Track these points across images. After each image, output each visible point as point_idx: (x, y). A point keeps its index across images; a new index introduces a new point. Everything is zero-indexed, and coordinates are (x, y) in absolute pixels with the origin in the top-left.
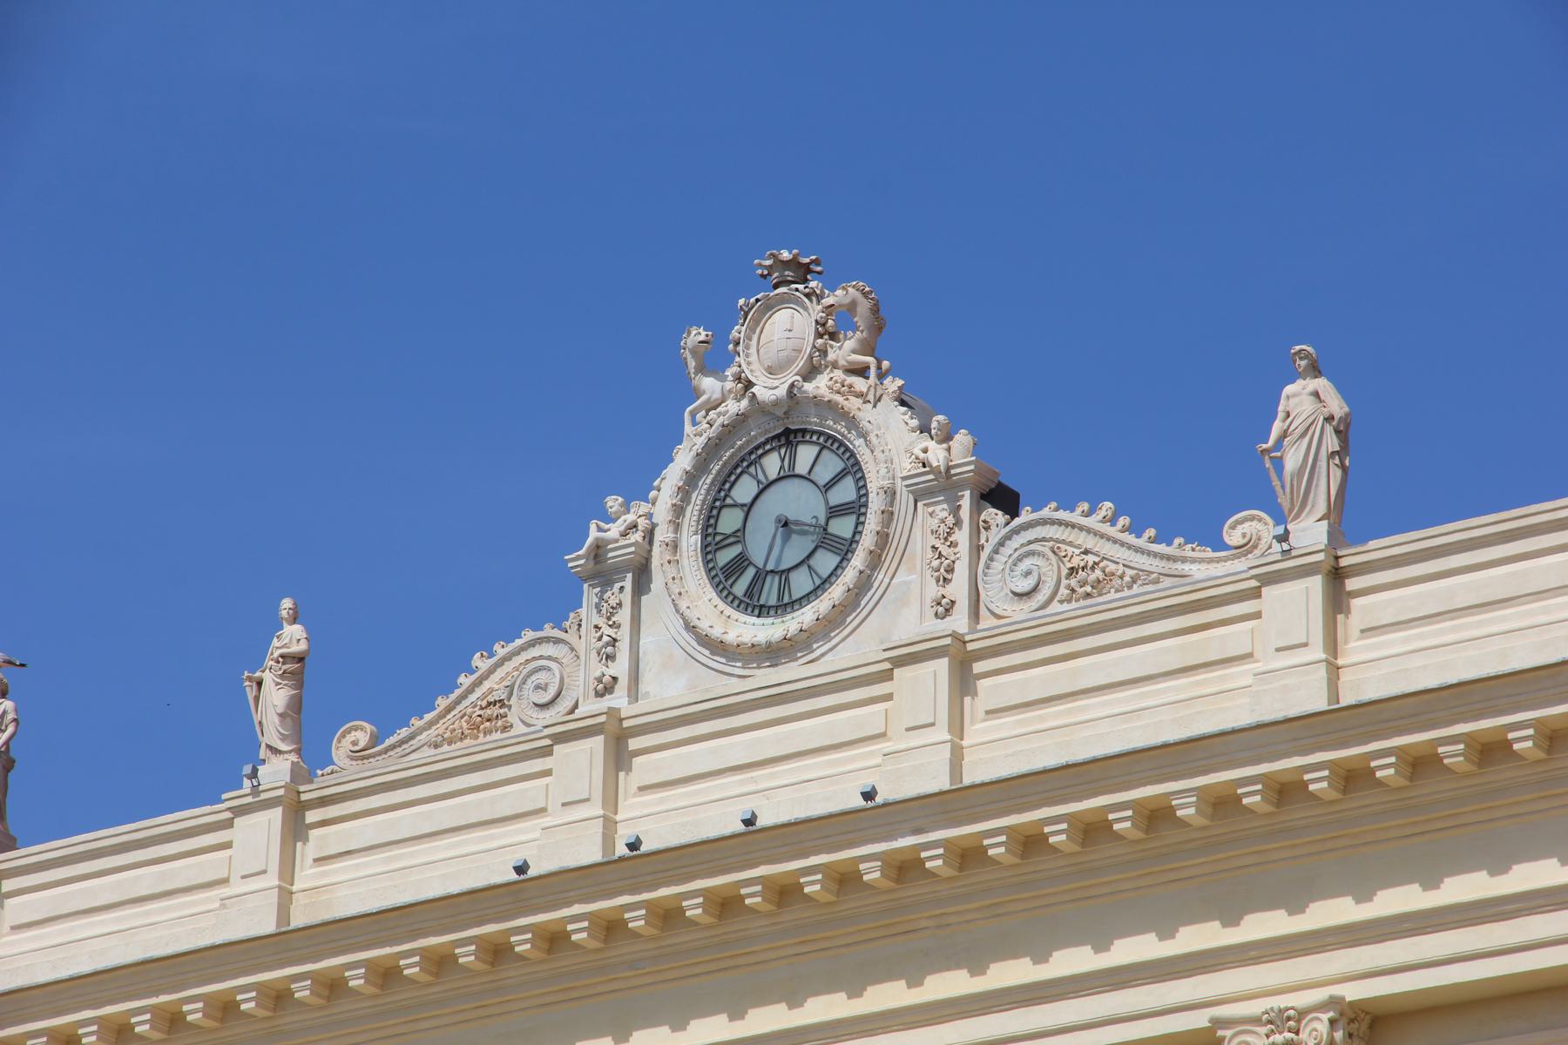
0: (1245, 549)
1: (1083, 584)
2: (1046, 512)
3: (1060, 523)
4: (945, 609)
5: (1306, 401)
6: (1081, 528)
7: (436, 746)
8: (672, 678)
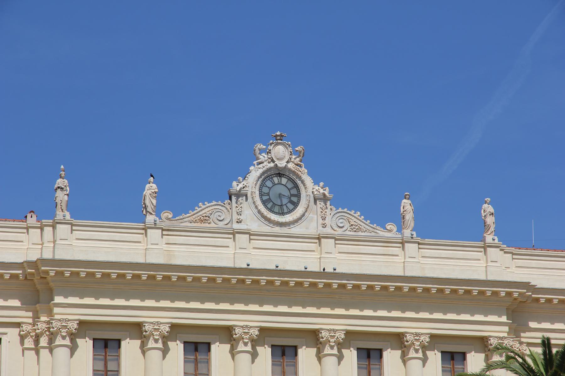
0: (390, 231)
1: (354, 228)
2: (345, 210)
3: (348, 213)
4: (324, 226)
5: (151, 188)
6: (353, 216)
7: (191, 222)
8: (252, 222)
